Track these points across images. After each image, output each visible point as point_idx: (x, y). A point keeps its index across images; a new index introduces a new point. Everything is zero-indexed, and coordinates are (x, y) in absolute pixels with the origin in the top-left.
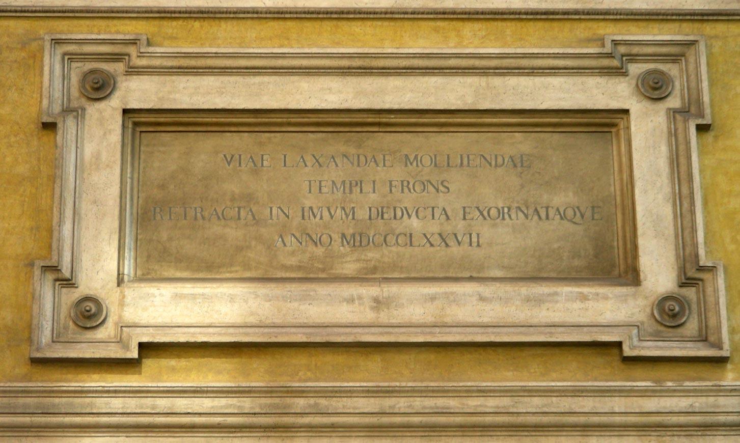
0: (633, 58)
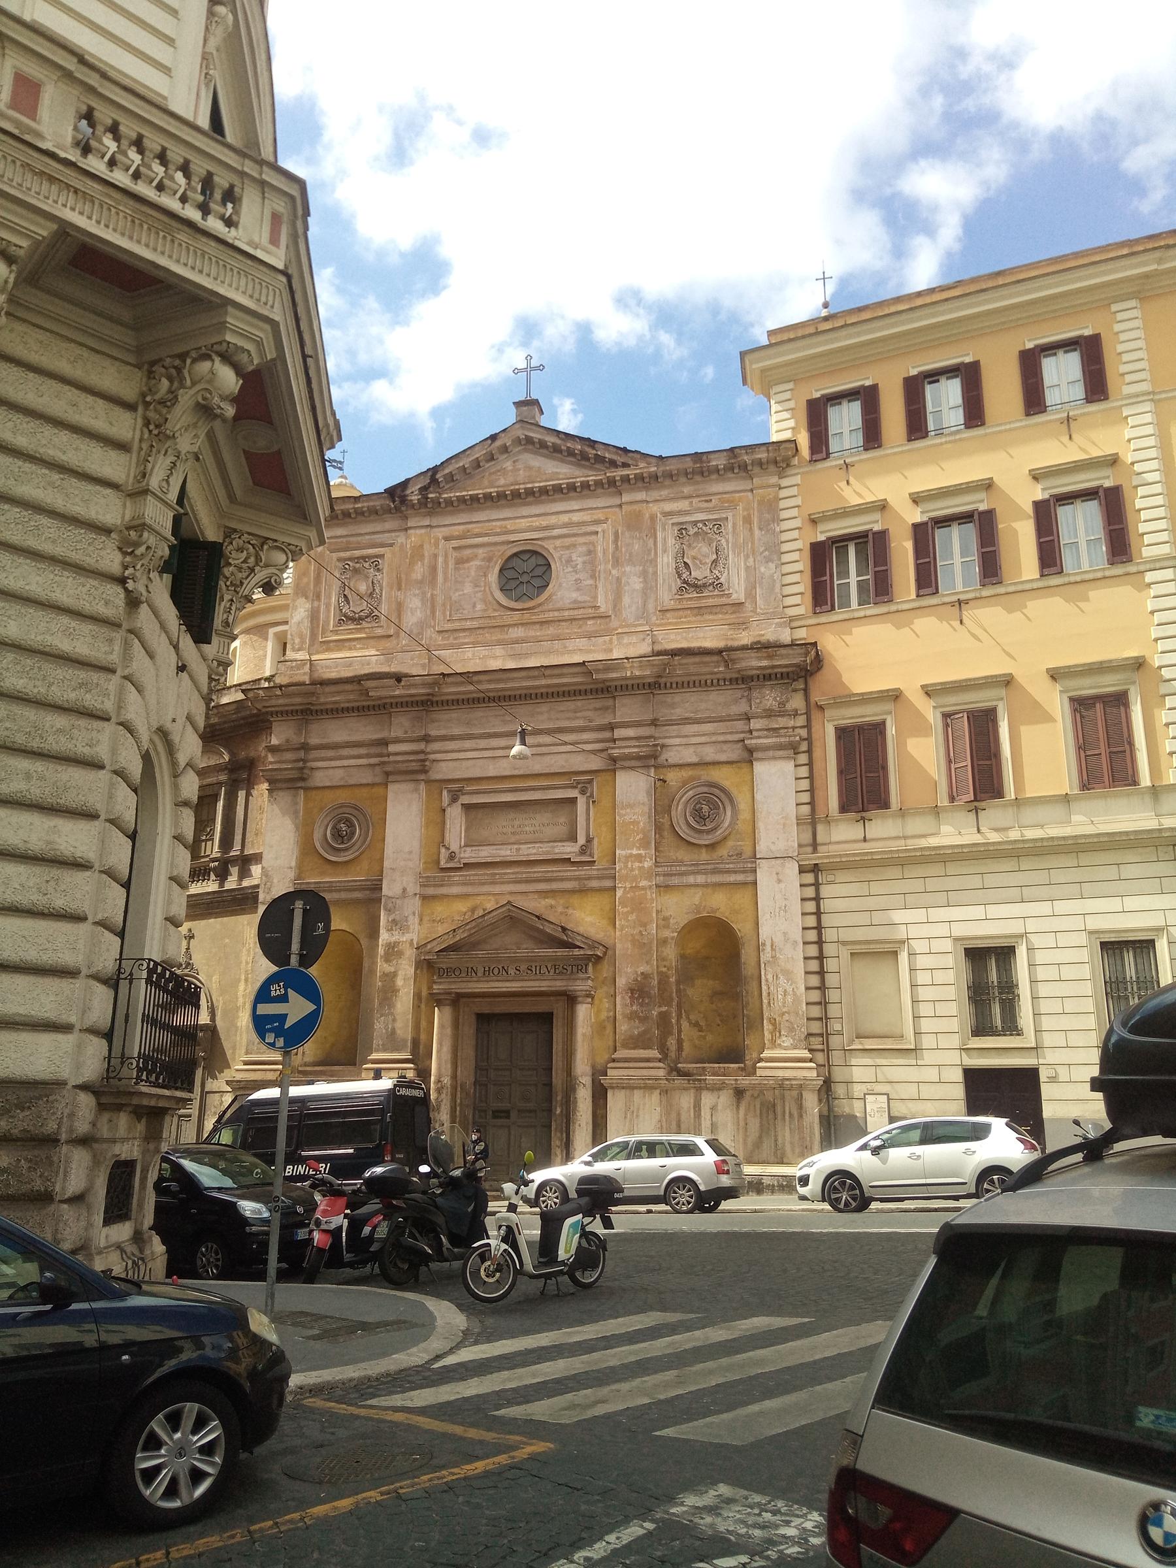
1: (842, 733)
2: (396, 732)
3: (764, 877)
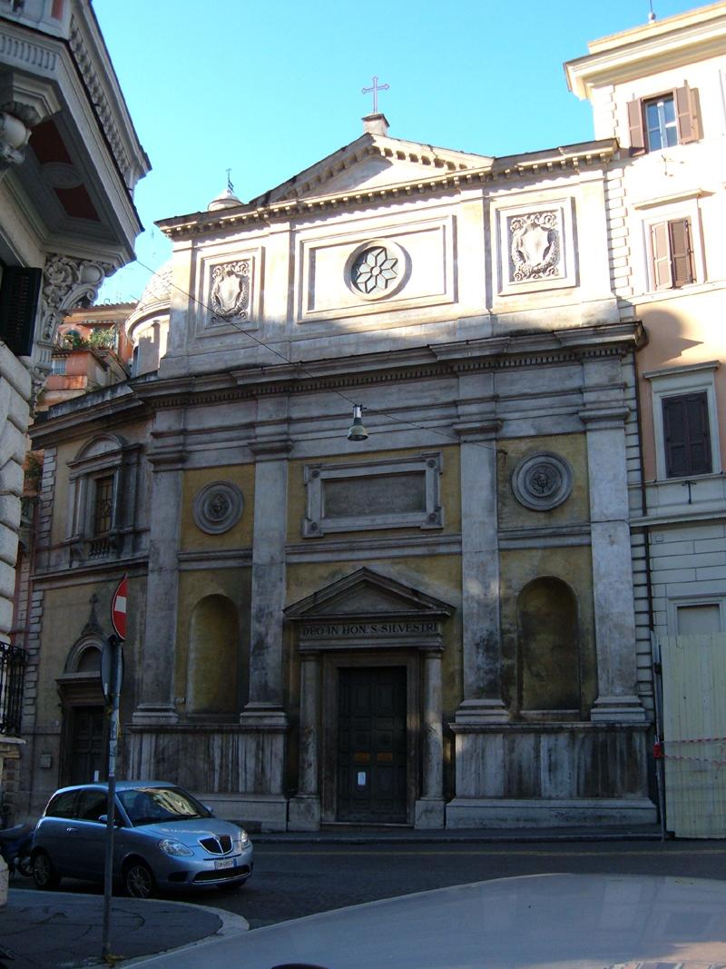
0: (428, 457)
1: (668, 404)
2: (262, 417)
3: (598, 538)
